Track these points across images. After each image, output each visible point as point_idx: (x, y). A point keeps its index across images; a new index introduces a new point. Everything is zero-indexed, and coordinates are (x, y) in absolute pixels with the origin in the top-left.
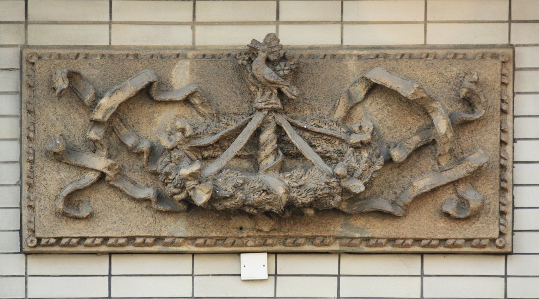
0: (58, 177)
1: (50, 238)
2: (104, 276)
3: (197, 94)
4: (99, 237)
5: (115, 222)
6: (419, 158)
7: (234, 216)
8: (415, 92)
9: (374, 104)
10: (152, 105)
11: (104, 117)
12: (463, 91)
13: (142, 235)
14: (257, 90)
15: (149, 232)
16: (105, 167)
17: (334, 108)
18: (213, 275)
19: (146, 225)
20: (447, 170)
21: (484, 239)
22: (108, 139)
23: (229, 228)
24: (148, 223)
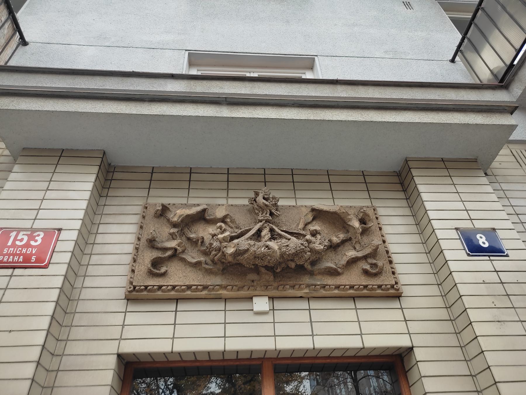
0: (151, 255)
1: (141, 286)
2: (172, 311)
3: (228, 216)
4: (171, 286)
5: (181, 278)
6: (344, 246)
7: (249, 274)
8: (340, 209)
9: (317, 224)
10: (205, 224)
11: (178, 220)
12: (250, 388)
13: (196, 284)
14: (259, 212)
15: (200, 282)
16: (177, 245)
17: (298, 225)
18: (237, 310)
19: (199, 279)
20: (360, 251)
21: (388, 285)
22: (181, 238)
23: (246, 280)
24: (200, 278)
